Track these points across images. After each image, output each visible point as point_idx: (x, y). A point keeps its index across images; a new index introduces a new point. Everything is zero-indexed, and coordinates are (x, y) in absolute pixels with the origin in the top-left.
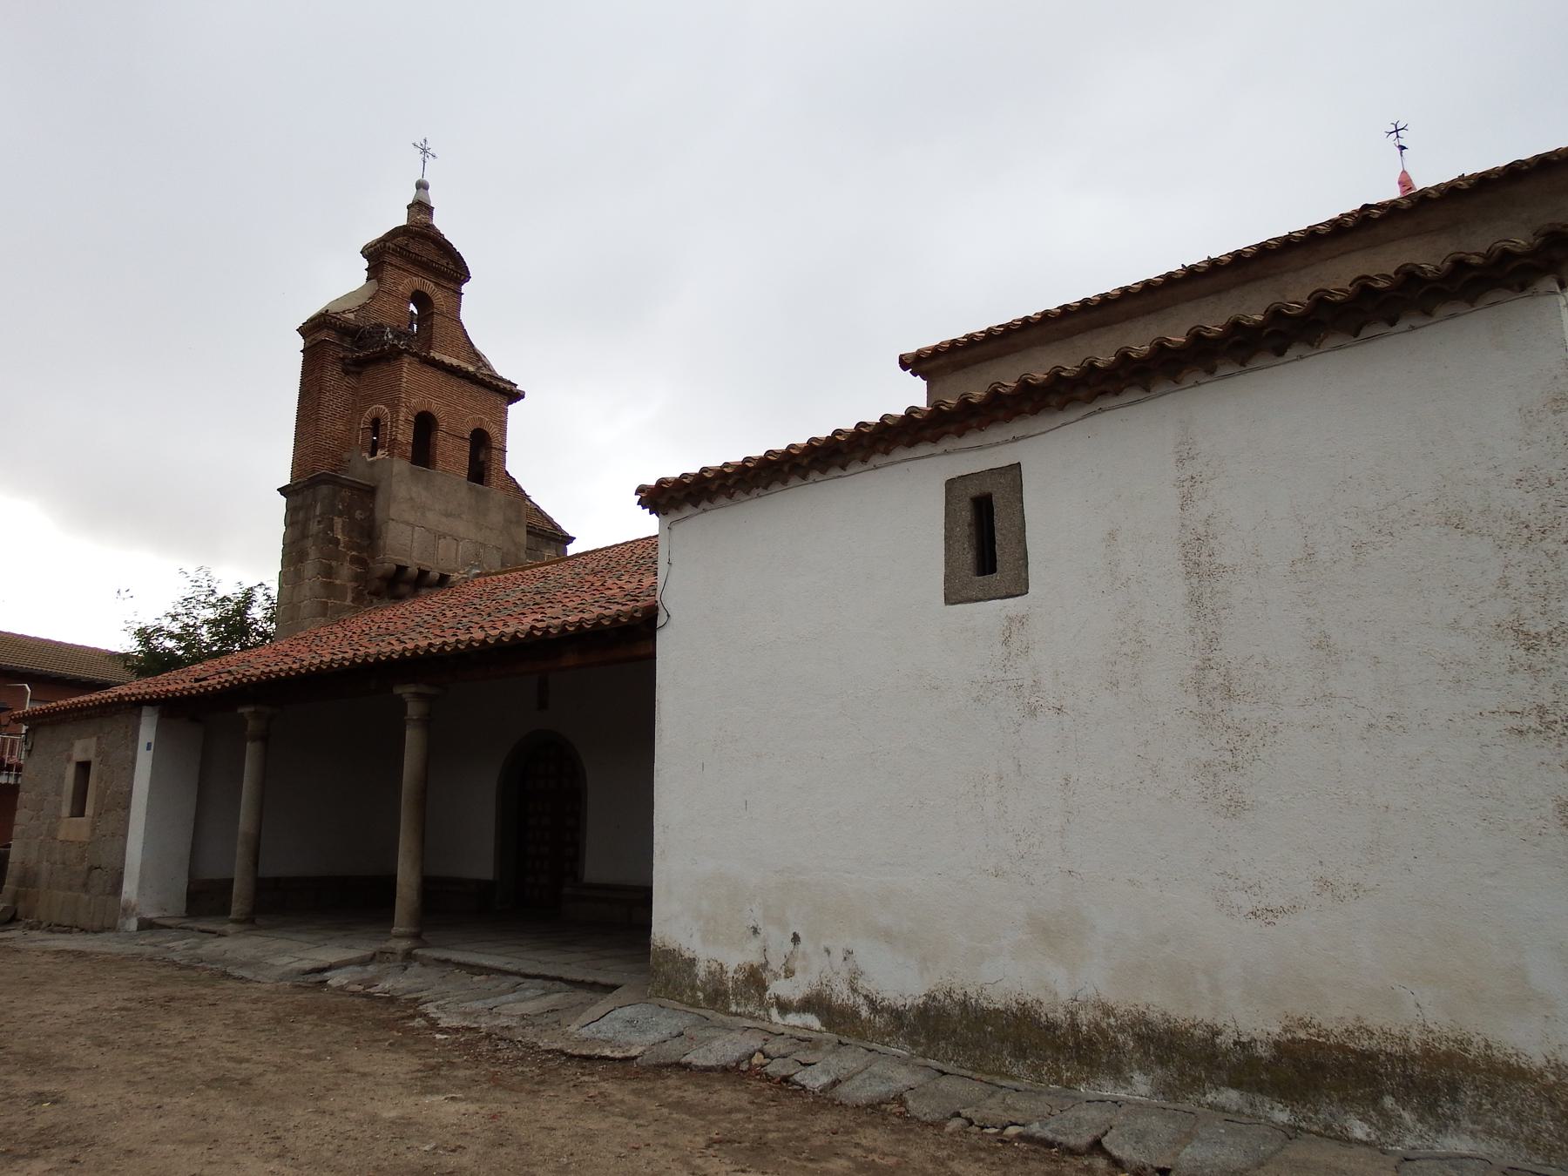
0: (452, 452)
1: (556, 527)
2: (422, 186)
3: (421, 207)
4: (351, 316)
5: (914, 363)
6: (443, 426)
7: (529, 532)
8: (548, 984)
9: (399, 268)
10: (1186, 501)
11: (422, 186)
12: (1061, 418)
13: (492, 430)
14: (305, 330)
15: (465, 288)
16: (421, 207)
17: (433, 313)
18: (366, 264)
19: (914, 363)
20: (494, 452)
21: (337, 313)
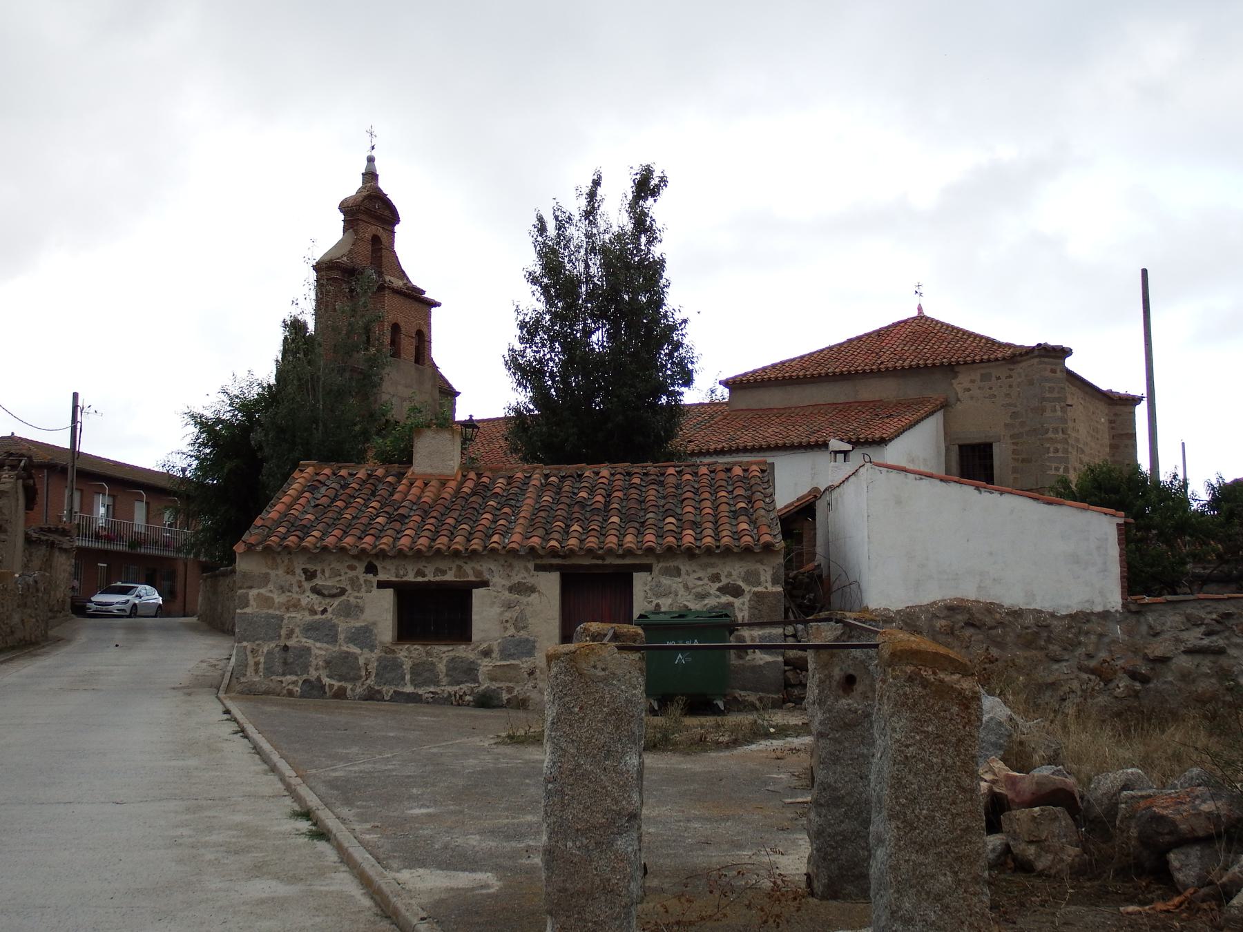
0: (408, 346)
1: (450, 386)
2: (371, 160)
3: (370, 176)
4: (345, 259)
5: (725, 383)
6: (403, 331)
7: (440, 391)
8: (917, 476)
9: (366, 222)
10: (813, 478)
11: (371, 160)
12: (785, 453)
13: (425, 330)
14: (318, 268)
15: (397, 228)
16: (370, 176)
17: (381, 249)
18: (342, 216)
19: (725, 383)
20: (426, 343)
21: (338, 259)
